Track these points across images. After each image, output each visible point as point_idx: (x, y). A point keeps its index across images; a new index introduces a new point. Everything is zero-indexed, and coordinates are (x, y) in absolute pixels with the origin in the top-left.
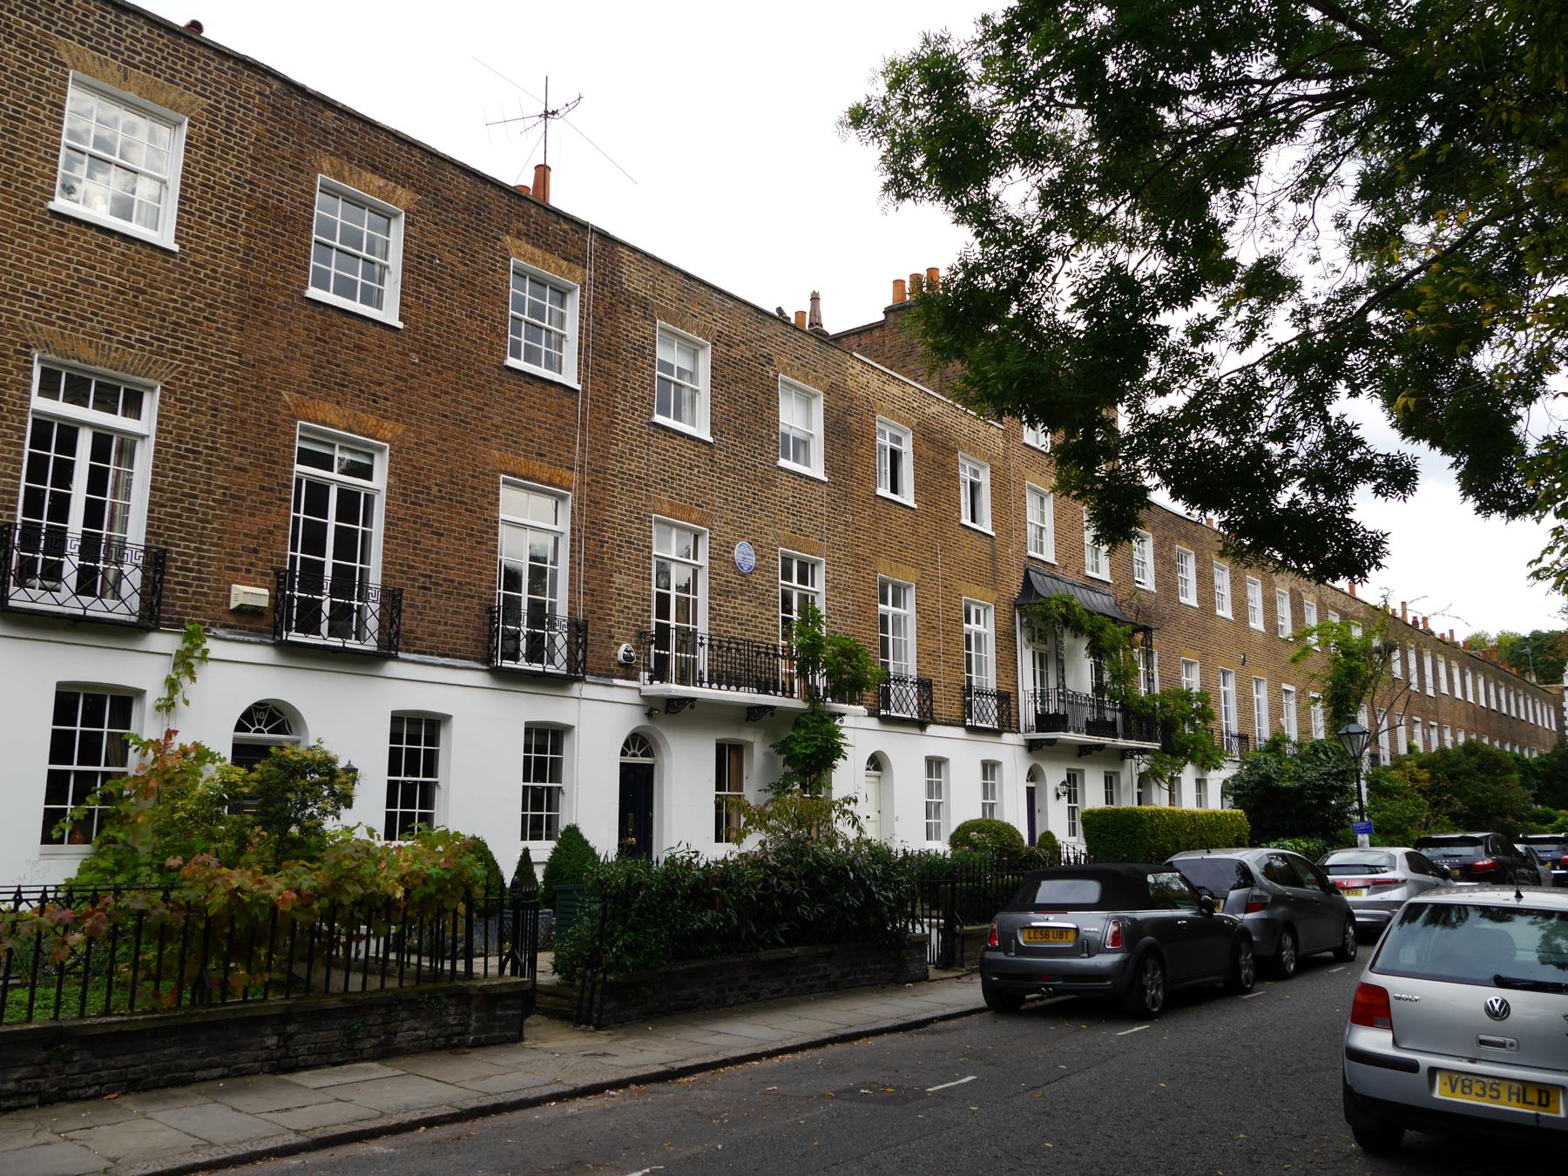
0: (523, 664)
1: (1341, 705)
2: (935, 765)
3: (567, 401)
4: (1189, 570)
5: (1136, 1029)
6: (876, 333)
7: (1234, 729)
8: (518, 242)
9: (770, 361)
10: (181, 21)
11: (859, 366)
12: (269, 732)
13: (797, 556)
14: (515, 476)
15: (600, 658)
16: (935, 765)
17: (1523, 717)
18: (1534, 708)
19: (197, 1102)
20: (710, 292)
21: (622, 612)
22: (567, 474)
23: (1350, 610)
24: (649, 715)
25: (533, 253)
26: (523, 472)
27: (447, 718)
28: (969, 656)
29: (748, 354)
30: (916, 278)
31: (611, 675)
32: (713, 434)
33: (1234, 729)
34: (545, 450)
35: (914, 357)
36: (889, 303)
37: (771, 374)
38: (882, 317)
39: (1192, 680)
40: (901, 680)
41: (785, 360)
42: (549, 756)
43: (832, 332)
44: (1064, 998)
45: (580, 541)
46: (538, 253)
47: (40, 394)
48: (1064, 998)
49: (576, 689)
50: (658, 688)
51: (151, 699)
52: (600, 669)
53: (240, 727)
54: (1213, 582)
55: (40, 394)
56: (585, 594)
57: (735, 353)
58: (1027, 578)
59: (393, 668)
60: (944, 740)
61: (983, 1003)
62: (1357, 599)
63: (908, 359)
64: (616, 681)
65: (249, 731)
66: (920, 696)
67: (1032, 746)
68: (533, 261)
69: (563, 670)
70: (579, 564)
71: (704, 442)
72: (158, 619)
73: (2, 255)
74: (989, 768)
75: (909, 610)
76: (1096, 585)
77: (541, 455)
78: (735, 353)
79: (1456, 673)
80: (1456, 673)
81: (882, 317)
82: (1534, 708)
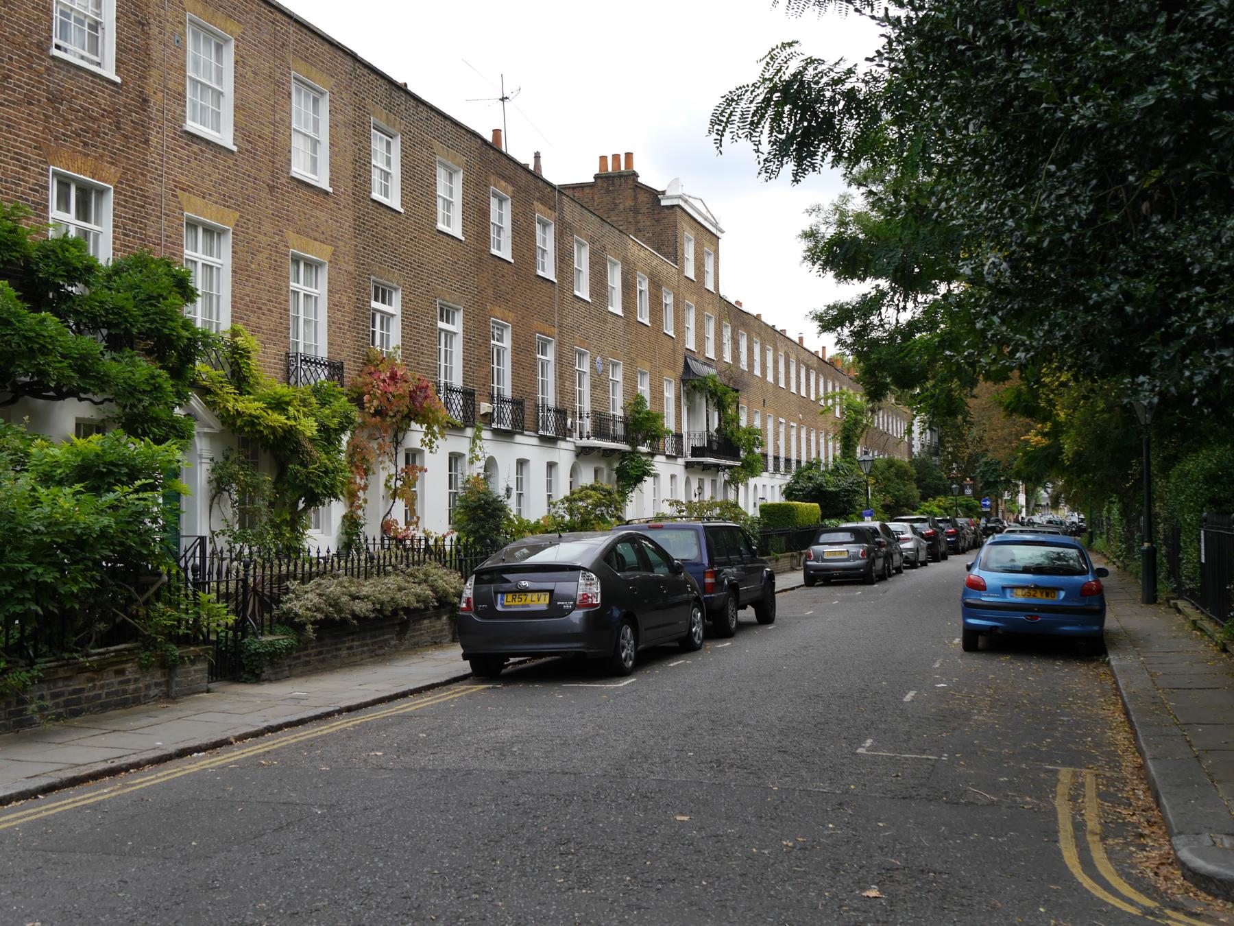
1: (848, 444)
2: (522, 463)
4: (546, 240)
5: (626, 683)
6: (587, 190)
10: (771, 324)
11: (631, 242)
16: (522, 463)
17: (548, 271)
18: (808, 379)
22: (553, 329)
23: (810, 363)
28: (374, 332)
30: (616, 157)
32: (623, 312)
35: (617, 212)
36: (597, 171)
38: (593, 180)
39: (757, 423)
40: (450, 389)
43: (556, 181)
44: (549, 659)
48: (549, 659)
50: (585, 442)
51: (467, 458)
58: (686, 362)
59: (518, 438)
60: (526, 446)
61: (469, 670)
62: (501, 152)
63: (612, 213)
66: (513, 412)
67: (688, 466)
69: (510, 428)
71: (585, 301)
72: (523, 428)
74: (551, 466)
75: (395, 307)
76: (710, 362)
79: (757, 349)
80: (757, 349)
81: (593, 180)
82: (808, 379)
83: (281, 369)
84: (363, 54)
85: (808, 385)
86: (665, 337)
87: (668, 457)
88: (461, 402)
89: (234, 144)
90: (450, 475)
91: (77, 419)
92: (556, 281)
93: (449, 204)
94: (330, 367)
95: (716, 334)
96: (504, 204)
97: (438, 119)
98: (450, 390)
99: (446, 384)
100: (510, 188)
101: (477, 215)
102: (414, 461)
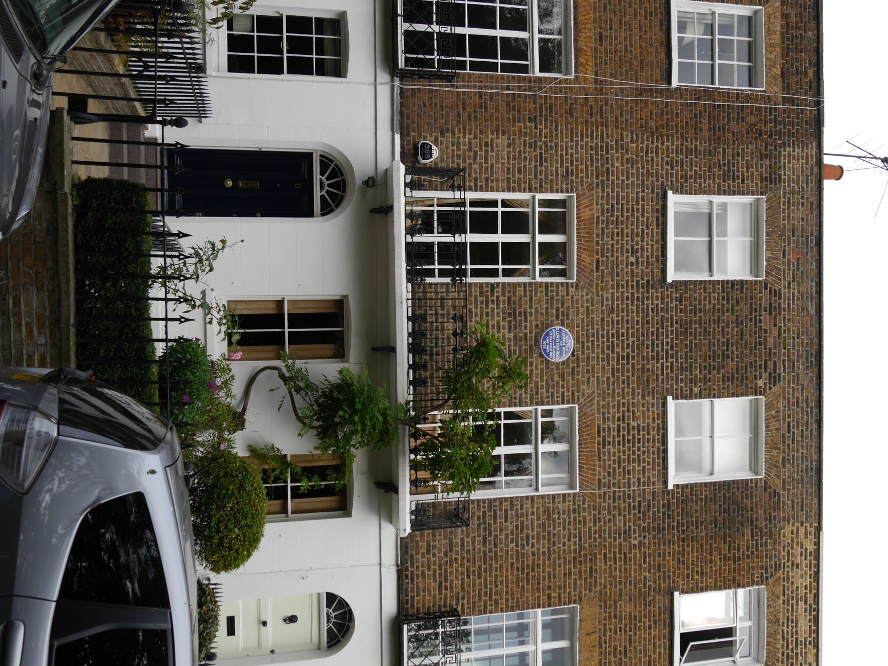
0: (402, 26)
3: (657, 73)
7: (472, 627)
8: (778, 14)
9: (774, 379)
12: (322, 197)
13: (570, 238)
14: (575, 8)
15: (419, 116)
19: (38, 489)
20: (816, 271)
21: (470, 149)
24: (370, 182)
25: (775, 32)
26: (581, 18)
27: (343, 14)
29: (770, 341)
31: (404, 132)
33: (472, 627)
34: (606, 43)
37: (760, 383)
41: (780, 405)
42: (314, 56)
45: (530, 89)
46: (777, 38)
47: (540, 233)
49: (384, 77)
52: (408, 118)
53: (326, 162)
54: (739, 586)
55: (540, 233)
56: (481, 94)
57: (765, 316)
64: (397, 137)
65: (322, 174)
68: (769, 32)
70: (508, 88)
73: (620, 664)
77: (601, 38)
78: (765, 316)
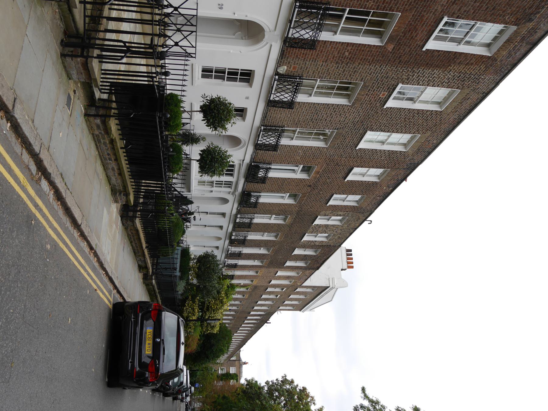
16: (221, 227)
32: (278, 276)
40: (252, 219)
83: (299, 51)
84: (420, 167)
85: (235, 341)
86: (329, 195)
87: (231, 235)
88: (285, 100)
89: (387, 107)
90: (223, 182)
91: (254, 71)
92: (270, 284)
93: (363, 175)
94: (256, 203)
95: (298, 267)
96: (377, 178)
97: (321, 262)
98: (257, 198)
99: (270, 168)
100: (449, 111)
101: (336, 210)
102: (237, 115)
